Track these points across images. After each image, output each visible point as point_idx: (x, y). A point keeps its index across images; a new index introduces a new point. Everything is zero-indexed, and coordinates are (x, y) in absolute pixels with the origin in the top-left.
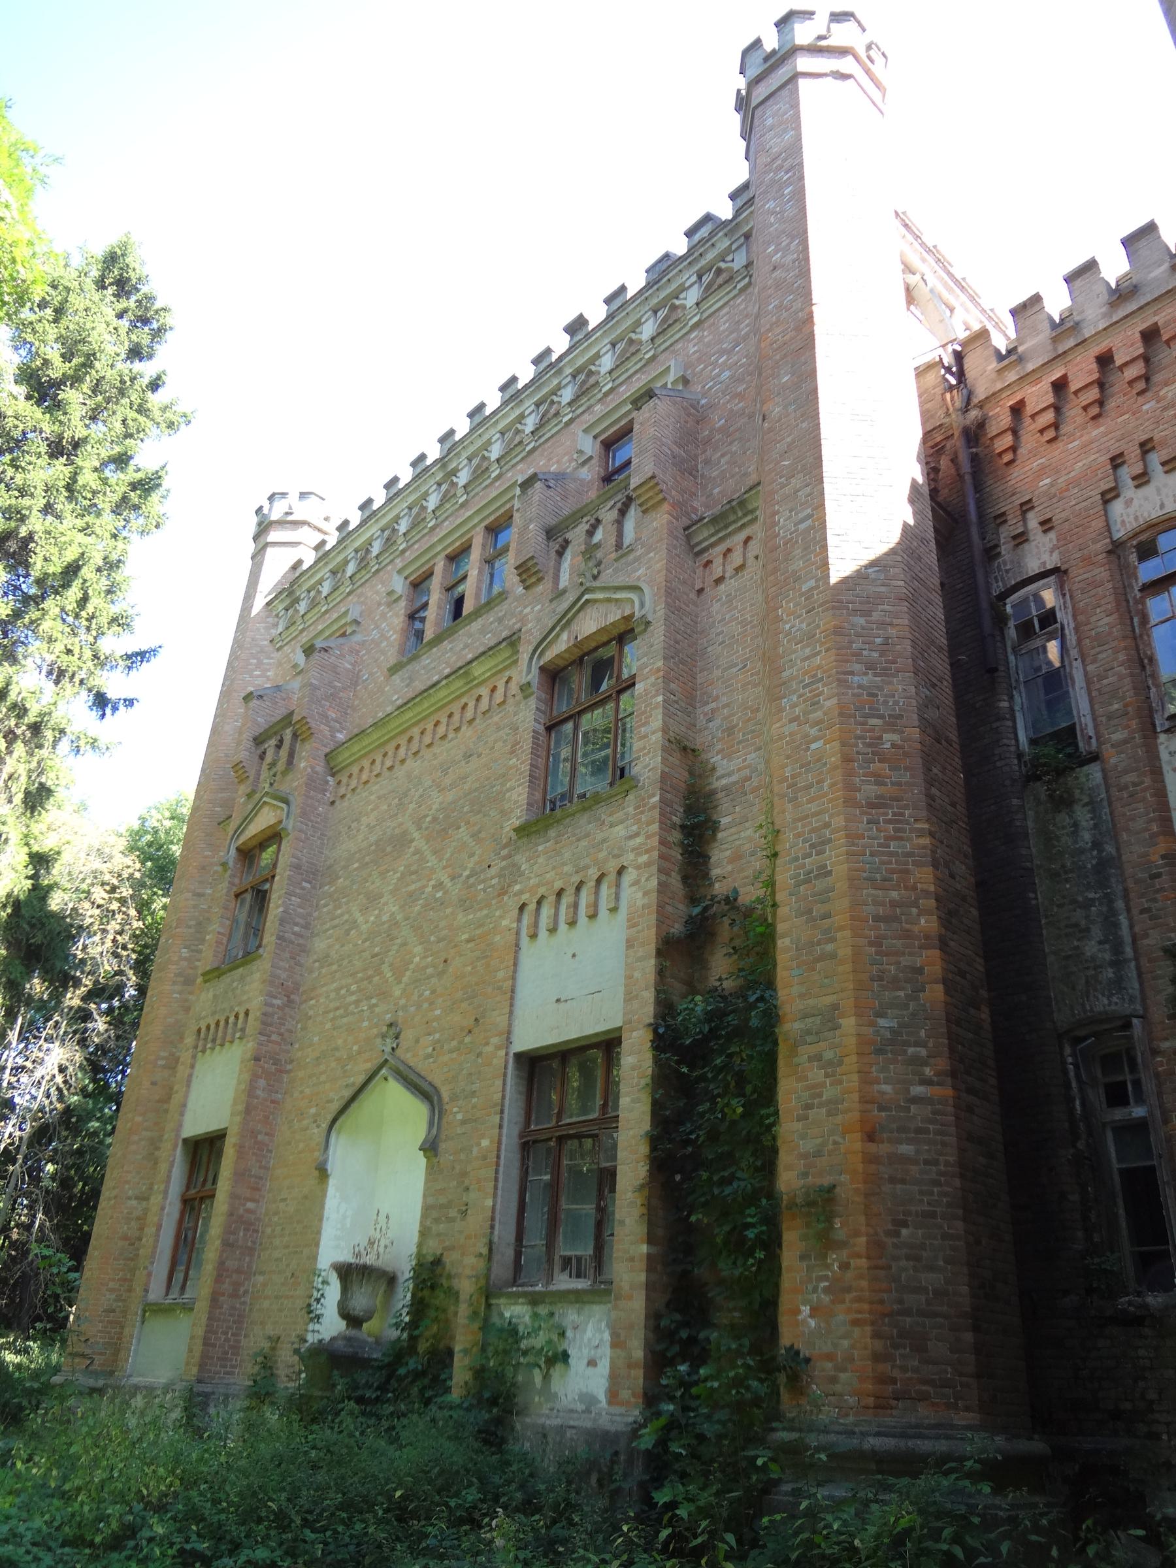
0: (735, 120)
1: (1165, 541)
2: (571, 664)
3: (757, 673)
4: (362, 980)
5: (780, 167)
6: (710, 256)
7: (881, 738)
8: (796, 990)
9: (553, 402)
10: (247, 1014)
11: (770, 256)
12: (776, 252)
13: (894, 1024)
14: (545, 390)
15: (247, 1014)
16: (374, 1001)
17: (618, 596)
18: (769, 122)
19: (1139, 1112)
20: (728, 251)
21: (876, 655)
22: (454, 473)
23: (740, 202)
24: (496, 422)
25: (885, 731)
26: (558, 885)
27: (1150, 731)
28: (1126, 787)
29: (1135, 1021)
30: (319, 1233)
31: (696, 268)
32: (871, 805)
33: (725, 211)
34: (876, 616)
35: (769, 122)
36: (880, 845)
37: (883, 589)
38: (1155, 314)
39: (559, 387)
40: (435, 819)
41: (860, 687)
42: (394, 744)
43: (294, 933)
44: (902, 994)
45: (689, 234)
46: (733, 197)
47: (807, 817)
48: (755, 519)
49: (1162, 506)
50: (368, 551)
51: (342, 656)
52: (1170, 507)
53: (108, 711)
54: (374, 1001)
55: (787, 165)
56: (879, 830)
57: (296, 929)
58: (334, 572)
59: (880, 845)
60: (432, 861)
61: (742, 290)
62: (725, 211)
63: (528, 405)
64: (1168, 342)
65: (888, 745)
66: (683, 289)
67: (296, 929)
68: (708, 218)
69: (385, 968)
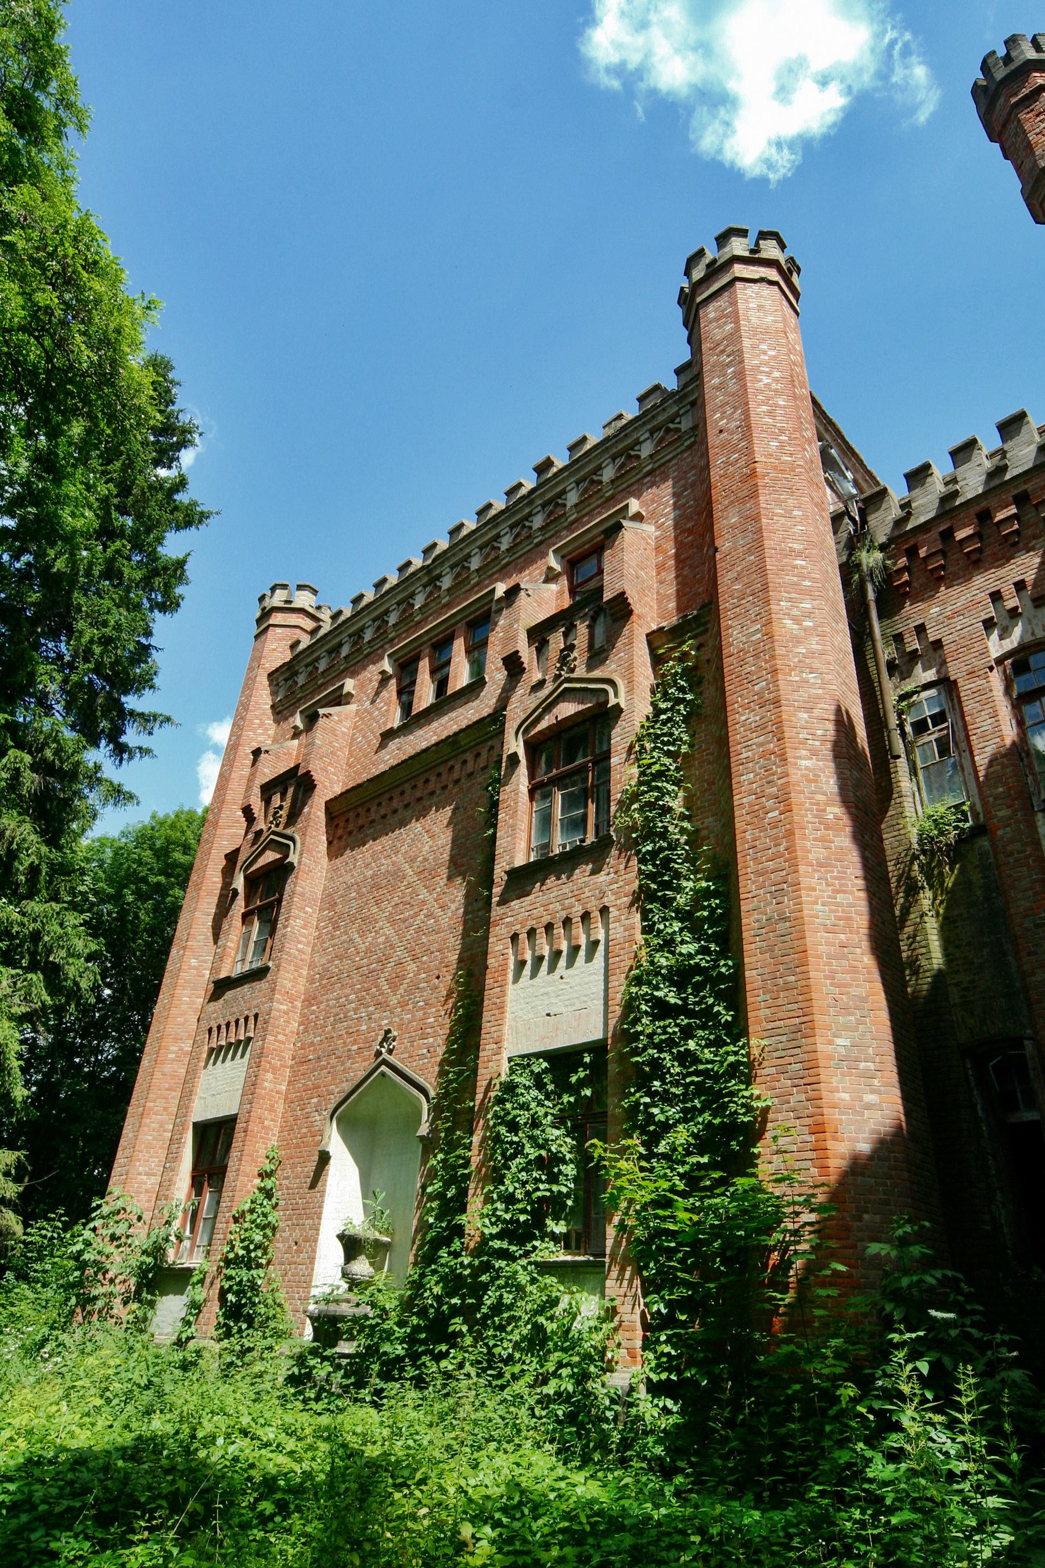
0: (678, 313)
1: (1034, 661)
2: (550, 739)
3: (712, 754)
4: (360, 990)
5: (723, 351)
6: (661, 418)
7: (825, 810)
8: (763, 1013)
9: (524, 526)
10: (256, 1016)
11: (717, 421)
12: (722, 418)
13: (847, 1043)
14: (519, 516)
15: (256, 1016)
16: (372, 1009)
17: (591, 686)
18: (712, 315)
19: (1030, 1116)
20: (677, 415)
21: (817, 743)
22: (439, 577)
23: (686, 377)
24: (475, 540)
25: (828, 805)
26: (546, 919)
27: (1029, 812)
28: (1012, 854)
29: (1026, 1042)
30: (321, 1207)
31: (649, 427)
32: (820, 865)
33: (671, 383)
34: (816, 712)
35: (712, 315)
36: (829, 897)
37: (820, 691)
38: (1025, 483)
39: (530, 515)
40: (426, 860)
41: (807, 768)
42: (387, 796)
43: (299, 950)
44: (852, 1018)
45: (641, 399)
46: (678, 372)
47: (767, 872)
48: (706, 631)
49: (1033, 634)
50: (361, 638)
51: (340, 721)
52: (1040, 634)
53: (125, 756)
54: (372, 1009)
55: (729, 349)
56: (827, 885)
57: (300, 946)
58: (329, 652)
59: (829, 897)
60: (424, 894)
61: (689, 447)
62: (671, 383)
63: (503, 528)
64: (1036, 506)
65: (831, 816)
66: (638, 442)
67: (300, 946)
68: (657, 388)
69: (382, 982)
